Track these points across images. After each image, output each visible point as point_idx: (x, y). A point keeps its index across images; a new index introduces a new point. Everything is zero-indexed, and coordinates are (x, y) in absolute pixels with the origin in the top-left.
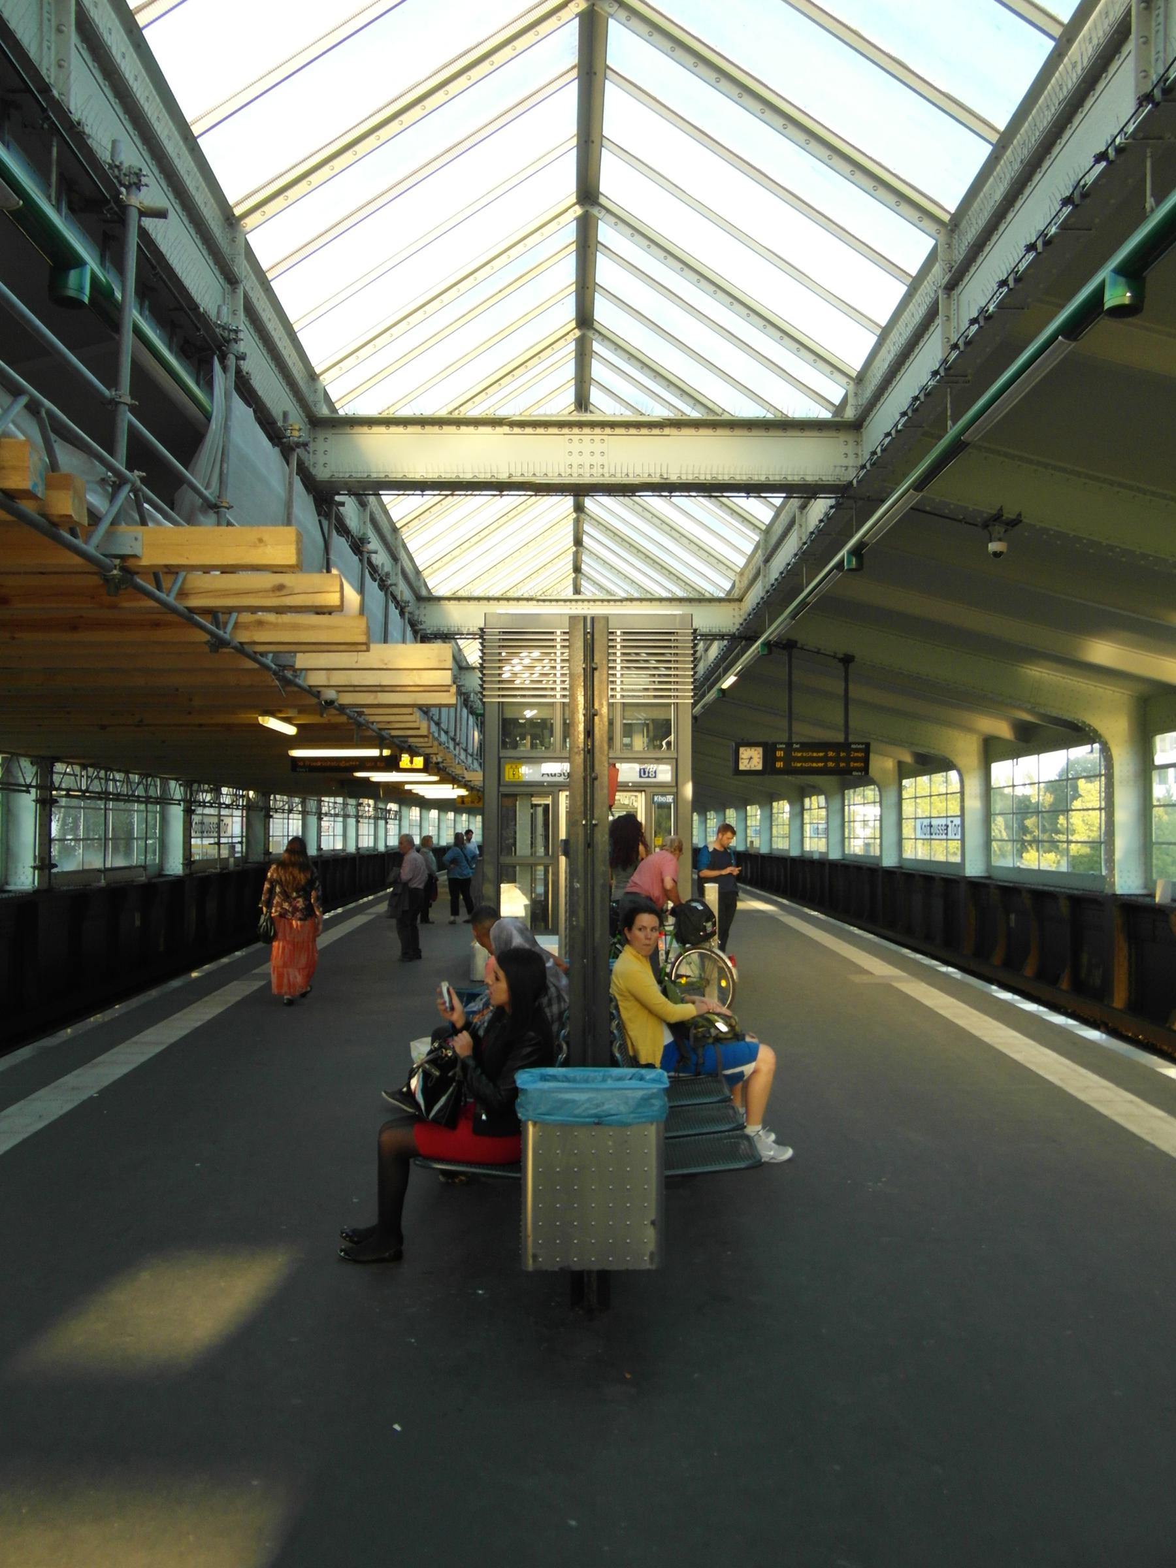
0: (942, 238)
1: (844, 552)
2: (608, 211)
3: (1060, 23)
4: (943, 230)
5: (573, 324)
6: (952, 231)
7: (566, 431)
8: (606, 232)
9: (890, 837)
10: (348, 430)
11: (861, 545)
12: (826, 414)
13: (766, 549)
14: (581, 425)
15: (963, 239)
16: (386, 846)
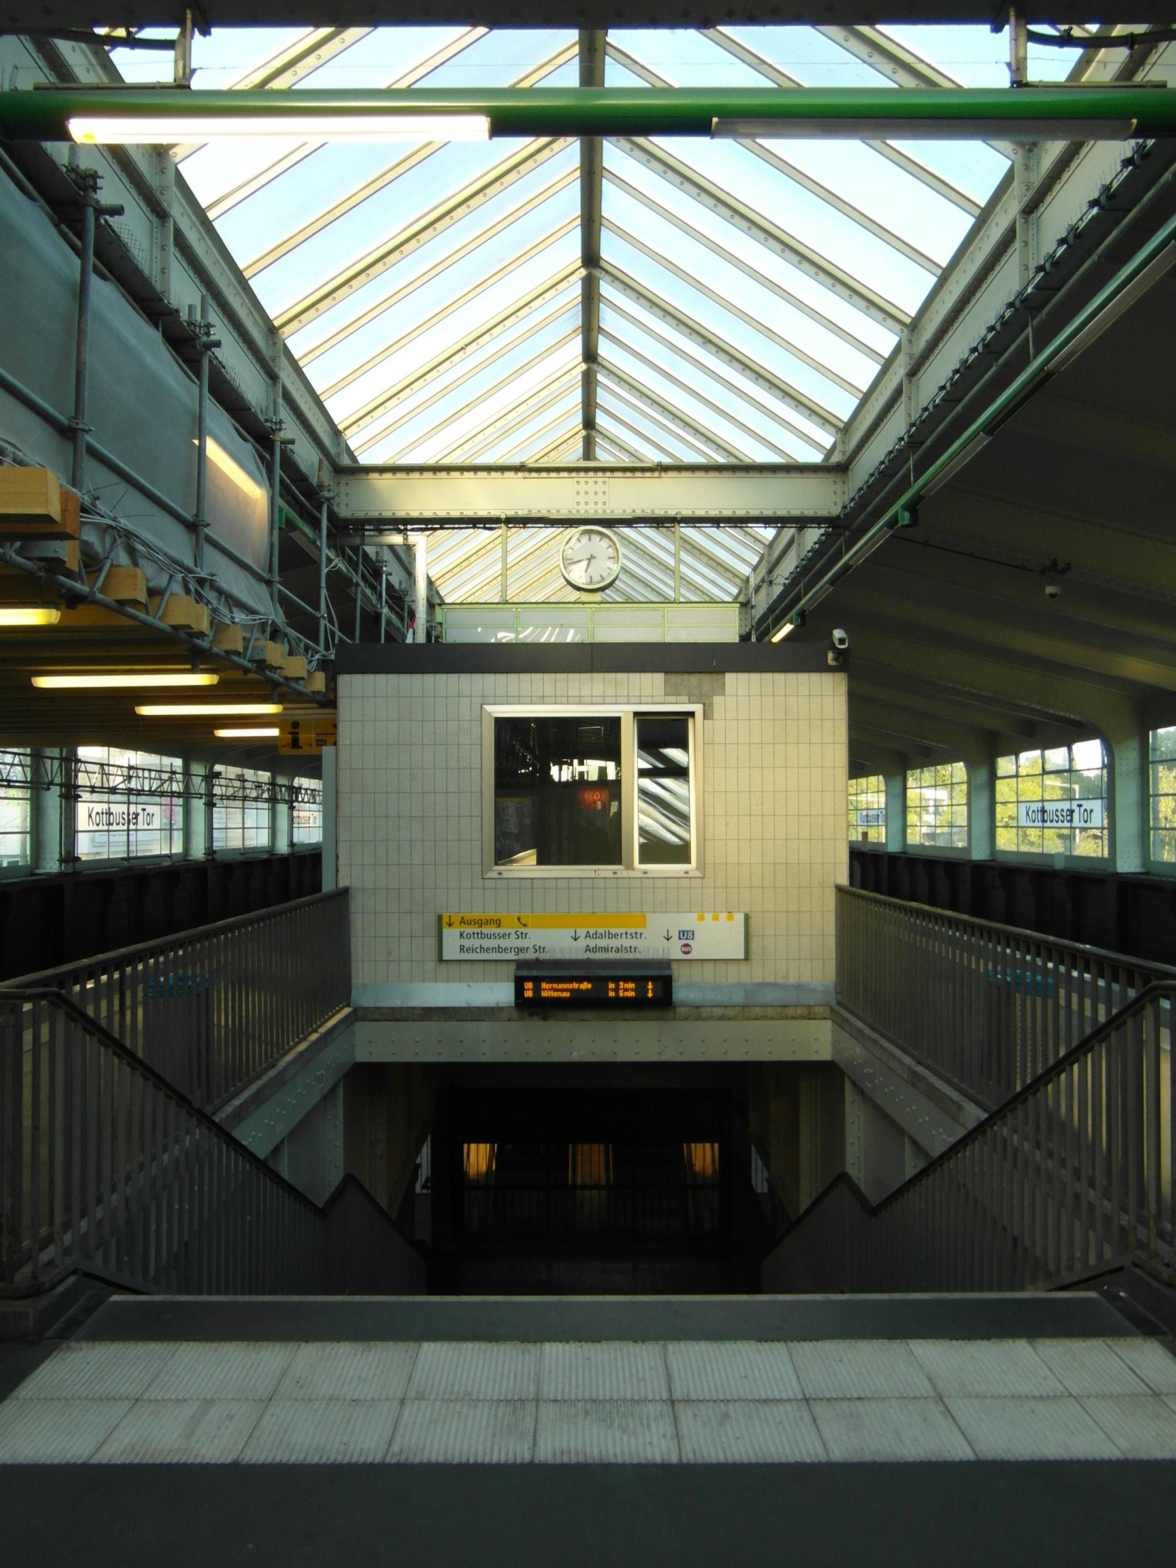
0: (1019, 158)
1: (897, 507)
2: (603, 367)
3: (978, 206)
4: (906, 330)
5: (581, 426)
6: (913, 330)
7: (574, 474)
8: (606, 289)
9: (981, 827)
10: (363, 476)
11: (918, 499)
12: (817, 458)
13: (769, 562)
14: (587, 470)
15: (921, 339)
16: (292, 844)
